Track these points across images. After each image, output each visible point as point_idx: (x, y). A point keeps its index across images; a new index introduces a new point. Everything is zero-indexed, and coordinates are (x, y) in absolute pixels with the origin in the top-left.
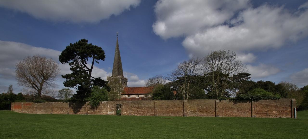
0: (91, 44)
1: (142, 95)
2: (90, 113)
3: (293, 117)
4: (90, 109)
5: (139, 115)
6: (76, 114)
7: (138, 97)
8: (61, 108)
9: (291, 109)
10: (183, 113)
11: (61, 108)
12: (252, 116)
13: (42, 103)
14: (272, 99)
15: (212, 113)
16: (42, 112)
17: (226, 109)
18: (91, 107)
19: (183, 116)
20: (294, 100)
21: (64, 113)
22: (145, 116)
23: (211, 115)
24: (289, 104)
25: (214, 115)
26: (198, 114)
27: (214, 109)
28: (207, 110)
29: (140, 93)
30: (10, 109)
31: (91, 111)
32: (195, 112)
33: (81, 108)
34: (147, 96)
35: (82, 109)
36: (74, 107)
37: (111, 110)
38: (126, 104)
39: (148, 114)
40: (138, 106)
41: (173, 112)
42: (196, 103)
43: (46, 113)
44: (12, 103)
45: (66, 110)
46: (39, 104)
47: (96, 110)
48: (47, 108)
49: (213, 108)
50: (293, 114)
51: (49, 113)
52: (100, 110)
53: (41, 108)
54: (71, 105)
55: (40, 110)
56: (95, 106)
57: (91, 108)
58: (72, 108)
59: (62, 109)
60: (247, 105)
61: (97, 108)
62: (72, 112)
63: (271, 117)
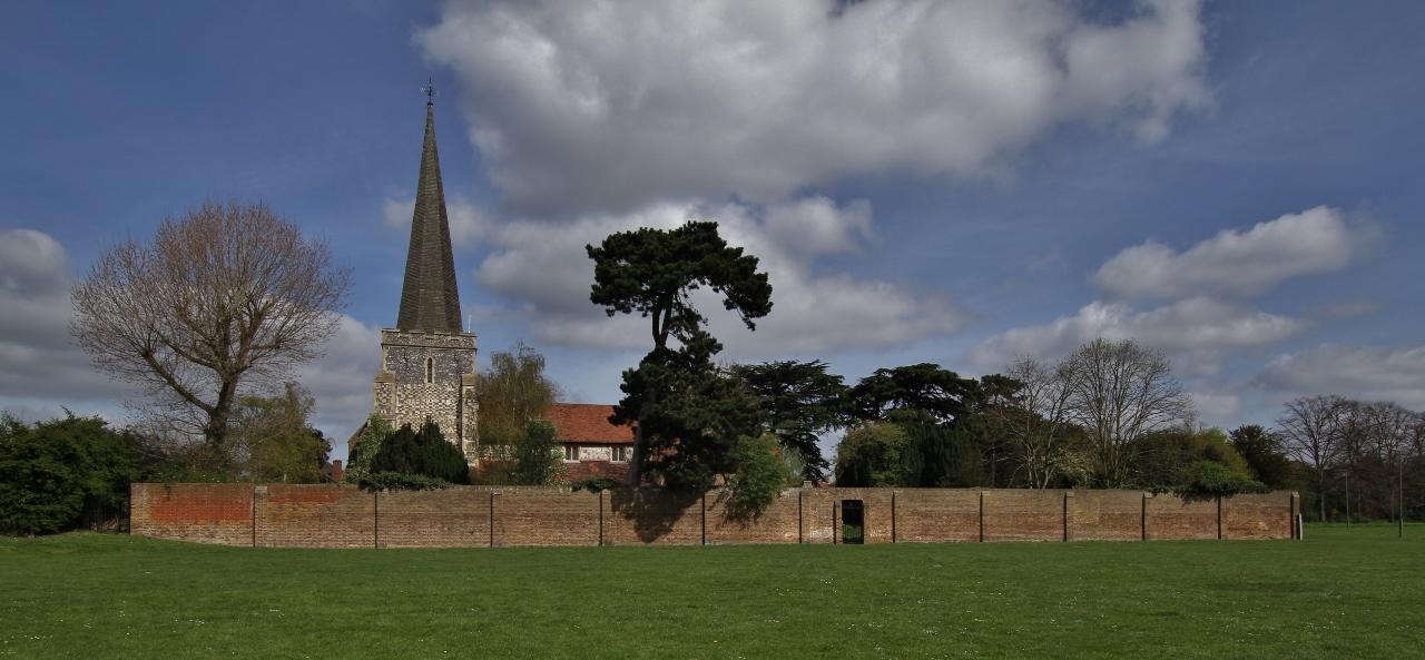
0: (716, 225)
1: (598, 450)
2: (724, 538)
3: (1295, 537)
4: (725, 522)
5: (928, 540)
6: (653, 544)
7: (576, 457)
8: (561, 515)
9: (1292, 517)
10: (1062, 532)
11: (558, 518)
12: (1220, 537)
13: (429, 493)
14: (1258, 493)
15: (1136, 529)
16: (432, 538)
17: (1167, 519)
18: (730, 510)
19: (1061, 540)
20: (1296, 495)
21: (586, 537)
22: (948, 542)
23: (1133, 535)
24: (1288, 506)
25: (1140, 534)
26: (1102, 535)
27: (1139, 519)
28: (1121, 521)
29: (584, 440)
30: (125, 527)
31: (730, 531)
32: (1093, 526)
33: (675, 516)
34: (622, 452)
35: (683, 519)
36: (636, 514)
37: (821, 524)
38: (879, 501)
39: (961, 537)
40: (924, 509)
41: (1036, 527)
42: (1097, 499)
43: (458, 541)
44: (135, 487)
45: (563, 523)
46: (405, 494)
47: (756, 523)
48: (466, 517)
49: (1137, 515)
50: (1295, 531)
51: (481, 540)
52: (775, 522)
53: (415, 518)
54: (621, 503)
55: (266, 525)
56: (748, 506)
57: (730, 518)
58: (629, 517)
59: (571, 521)
60: (1209, 507)
61: (758, 515)
62: (625, 534)
63: (1256, 537)
